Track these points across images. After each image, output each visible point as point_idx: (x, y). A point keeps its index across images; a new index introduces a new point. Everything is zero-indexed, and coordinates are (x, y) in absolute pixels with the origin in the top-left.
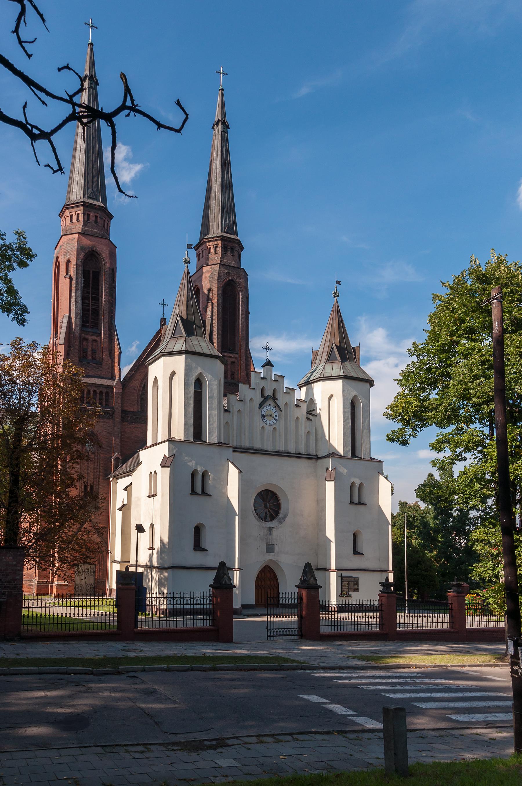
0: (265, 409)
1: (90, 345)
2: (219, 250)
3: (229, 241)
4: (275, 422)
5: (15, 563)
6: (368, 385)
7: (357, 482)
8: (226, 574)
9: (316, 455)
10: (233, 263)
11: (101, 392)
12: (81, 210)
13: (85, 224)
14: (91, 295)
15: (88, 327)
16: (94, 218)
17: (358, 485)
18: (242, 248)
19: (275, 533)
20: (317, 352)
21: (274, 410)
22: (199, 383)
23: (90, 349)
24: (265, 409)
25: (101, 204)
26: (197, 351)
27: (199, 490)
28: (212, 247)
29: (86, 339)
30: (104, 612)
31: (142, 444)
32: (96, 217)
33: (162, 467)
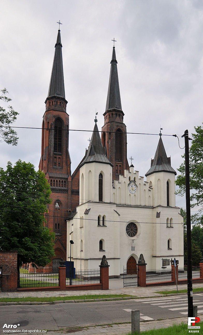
1: (57, 160)
3: (118, 112)
4: (135, 192)
5: (13, 258)
6: (174, 174)
7: (102, 215)
9: (153, 207)
10: (119, 121)
11: (62, 181)
14: (58, 137)
15: (56, 152)
16: (59, 103)
17: (170, 219)
18: (124, 115)
19: (135, 242)
21: (135, 187)
22: (101, 175)
31: (78, 205)
32: (60, 102)
33: (85, 214)
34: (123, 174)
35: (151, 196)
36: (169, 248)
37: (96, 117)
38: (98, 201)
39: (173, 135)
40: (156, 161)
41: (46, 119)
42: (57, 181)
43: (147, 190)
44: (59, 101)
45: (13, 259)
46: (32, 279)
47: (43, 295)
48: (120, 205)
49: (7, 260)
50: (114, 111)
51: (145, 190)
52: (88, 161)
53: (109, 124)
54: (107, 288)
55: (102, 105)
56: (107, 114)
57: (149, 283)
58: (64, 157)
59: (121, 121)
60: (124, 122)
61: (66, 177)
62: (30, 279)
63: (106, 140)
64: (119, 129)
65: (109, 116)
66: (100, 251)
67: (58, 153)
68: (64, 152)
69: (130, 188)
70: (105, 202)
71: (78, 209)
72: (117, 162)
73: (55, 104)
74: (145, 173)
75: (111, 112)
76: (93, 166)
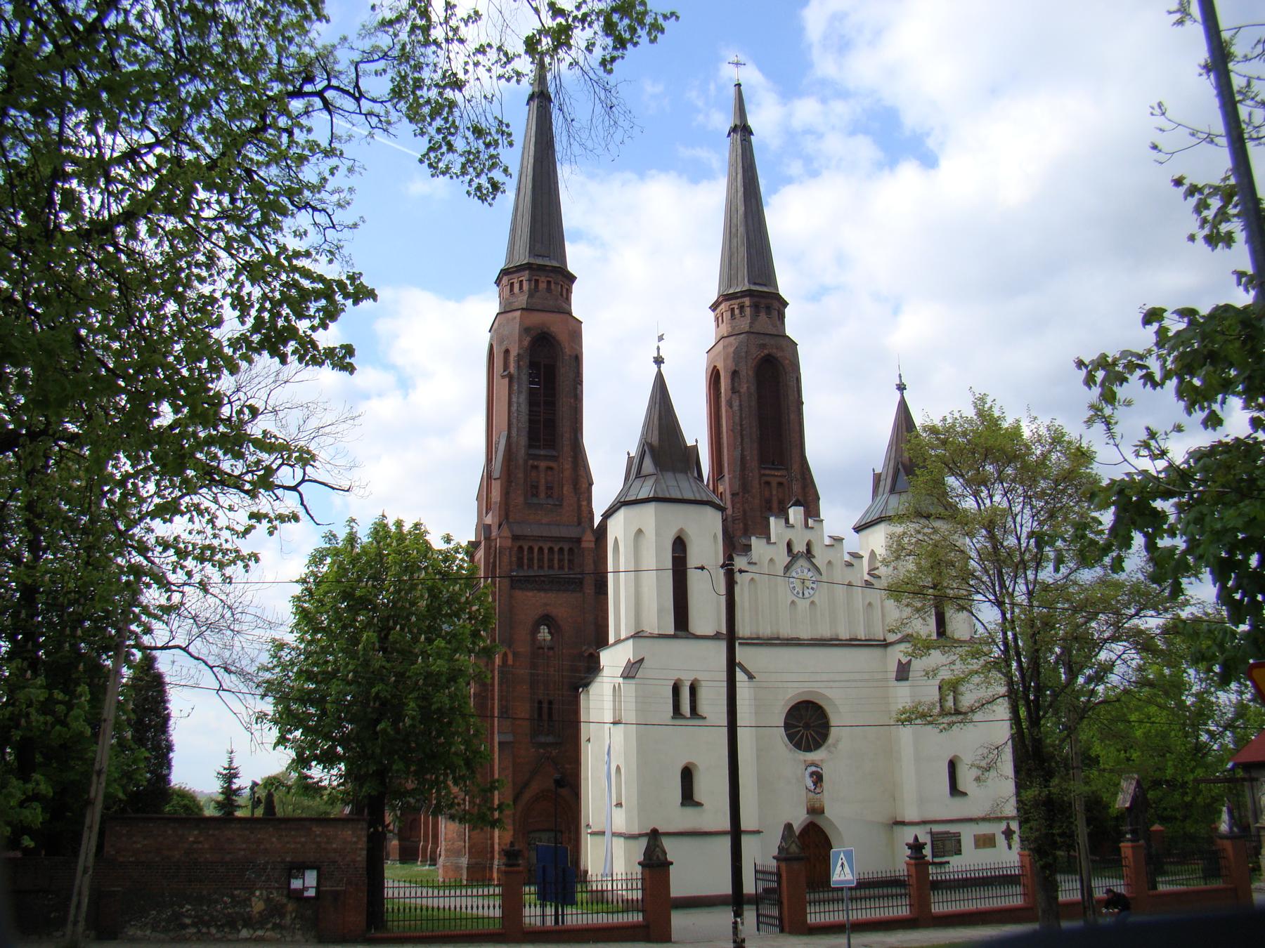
1: (542, 475)
2: (748, 311)
11: (561, 550)
12: (525, 276)
13: (531, 295)
15: (539, 447)
22: (680, 545)
25: (555, 264)
27: (686, 708)
31: (603, 642)
32: (549, 282)
37: (658, 348)
38: (672, 632)
41: (501, 341)
42: (541, 549)
45: (356, 843)
46: (436, 905)
48: (758, 638)
50: (752, 297)
55: (703, 272)
56: (723, 306)
58: (568, 466)
59: (775, 326)
60: (789, 332)
61: (573, 532)
62: (430, 904)
64: (769, 355)
66: (683, 804)
67: (542, 452)
68: (567, 449)
70: (698, 633)
71: (605, 657)
72: (767, 472)
73: (530, 290)
74: (855, 519)
76: (647, 516)
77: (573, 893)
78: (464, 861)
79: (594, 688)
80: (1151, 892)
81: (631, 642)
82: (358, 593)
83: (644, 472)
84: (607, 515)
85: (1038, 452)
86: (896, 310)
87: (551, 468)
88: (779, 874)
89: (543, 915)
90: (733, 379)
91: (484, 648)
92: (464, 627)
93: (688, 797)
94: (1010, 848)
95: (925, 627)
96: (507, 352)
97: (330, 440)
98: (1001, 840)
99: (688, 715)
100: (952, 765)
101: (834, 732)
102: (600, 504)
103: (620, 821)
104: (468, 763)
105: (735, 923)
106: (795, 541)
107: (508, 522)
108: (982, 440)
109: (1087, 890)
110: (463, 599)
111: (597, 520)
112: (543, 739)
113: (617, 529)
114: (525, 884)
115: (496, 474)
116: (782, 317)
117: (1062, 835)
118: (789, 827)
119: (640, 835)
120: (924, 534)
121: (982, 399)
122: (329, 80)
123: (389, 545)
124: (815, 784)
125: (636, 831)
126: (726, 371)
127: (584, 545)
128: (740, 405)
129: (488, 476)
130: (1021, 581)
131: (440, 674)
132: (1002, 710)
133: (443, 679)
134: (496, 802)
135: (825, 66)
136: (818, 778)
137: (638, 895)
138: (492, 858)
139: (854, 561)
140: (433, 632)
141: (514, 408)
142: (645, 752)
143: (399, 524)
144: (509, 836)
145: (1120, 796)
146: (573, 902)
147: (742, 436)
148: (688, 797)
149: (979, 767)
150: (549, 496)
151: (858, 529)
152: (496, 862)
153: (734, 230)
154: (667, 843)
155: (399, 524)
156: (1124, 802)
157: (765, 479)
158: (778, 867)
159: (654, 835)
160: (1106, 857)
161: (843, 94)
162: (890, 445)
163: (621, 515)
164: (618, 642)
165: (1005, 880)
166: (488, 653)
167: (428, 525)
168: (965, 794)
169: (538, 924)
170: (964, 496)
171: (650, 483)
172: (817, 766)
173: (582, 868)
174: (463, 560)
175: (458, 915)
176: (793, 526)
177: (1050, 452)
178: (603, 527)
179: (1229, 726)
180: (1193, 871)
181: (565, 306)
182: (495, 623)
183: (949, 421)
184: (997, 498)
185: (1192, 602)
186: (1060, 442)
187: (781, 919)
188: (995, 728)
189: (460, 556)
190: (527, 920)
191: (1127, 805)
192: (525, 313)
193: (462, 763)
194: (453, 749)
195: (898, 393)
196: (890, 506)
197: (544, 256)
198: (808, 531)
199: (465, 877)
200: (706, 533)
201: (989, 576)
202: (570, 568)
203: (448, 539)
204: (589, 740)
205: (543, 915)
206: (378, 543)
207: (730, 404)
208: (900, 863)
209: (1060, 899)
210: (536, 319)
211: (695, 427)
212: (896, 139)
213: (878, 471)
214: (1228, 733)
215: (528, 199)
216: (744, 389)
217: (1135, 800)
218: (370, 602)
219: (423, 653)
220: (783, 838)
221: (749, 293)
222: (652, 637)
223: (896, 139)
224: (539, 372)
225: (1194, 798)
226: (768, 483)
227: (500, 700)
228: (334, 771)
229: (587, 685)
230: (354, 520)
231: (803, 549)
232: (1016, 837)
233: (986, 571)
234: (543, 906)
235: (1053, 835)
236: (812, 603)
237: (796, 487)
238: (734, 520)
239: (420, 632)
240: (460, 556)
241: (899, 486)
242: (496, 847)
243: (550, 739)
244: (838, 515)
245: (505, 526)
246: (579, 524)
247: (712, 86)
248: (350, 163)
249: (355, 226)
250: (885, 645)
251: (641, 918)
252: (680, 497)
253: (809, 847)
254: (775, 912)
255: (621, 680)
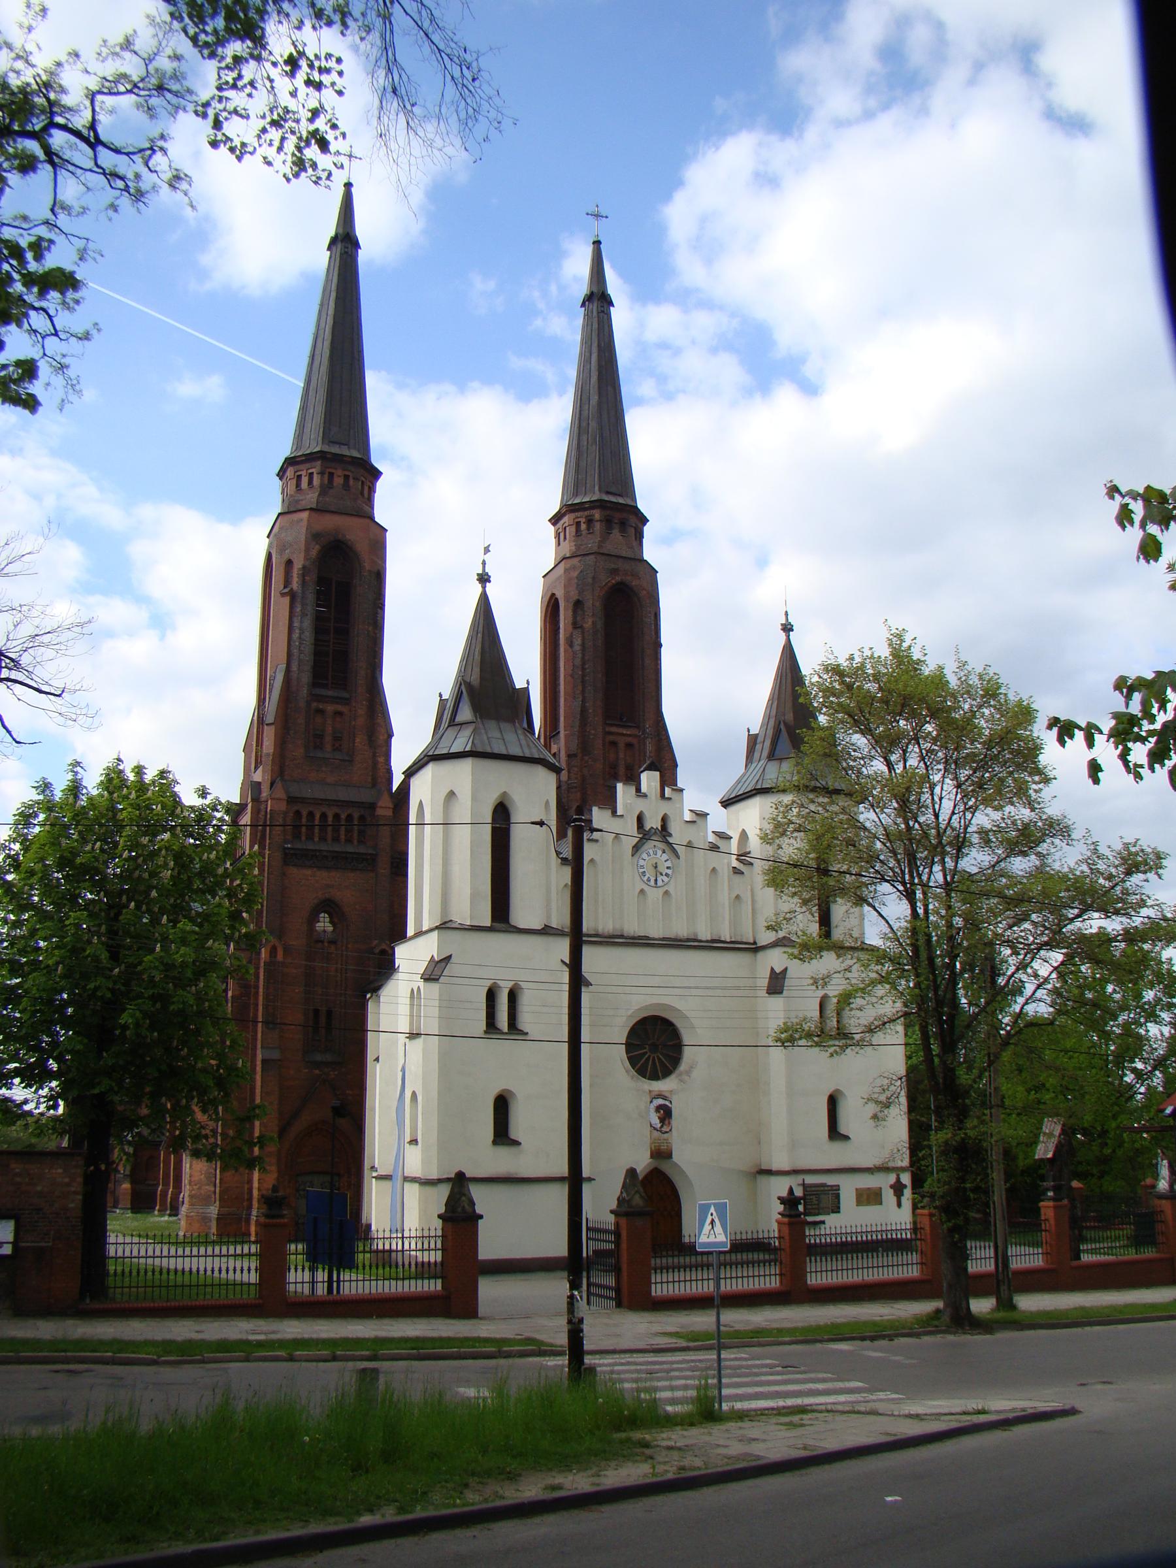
0: (645, 856)
1: (329, 722)
2: (597, 526)
5: (67, 1180)
8: (464, 1195)
9: (755, 943)
10: (629, 554)
11: (349, 818)
13: (324, 490)
20: (756, 736)
22: (502, 814)
23: (329, 729)
24: (645, 856)
25: (355, 454)
26: (496, 751)
28: (583, 520)
29: (320, 712)
30: (388, 1269)
31: (400, 935)
32: (346, 477)
34: (610, 802)
35: (747, 897)
36: (835, 1133)
37: (484, 563)
38: (487, 922)
39: (533, 823)
40: (768, 743)
42: (324, 816)
43: (725, 873)
44: (339, 472)
46: (172, 1267)
47: (182, 1330)
48: (596, 935)
49: (39, 1188)
50: (602, 509)
51: (714, 869)
52: (445, 751)
53: (575, 561)
54: (470, 1311)
57: (734, 1287)
58: (362, 711)
60: (648, 555)
61: (365, 796)
63: (562, 631)
64: (622, 583)
65: (573, 529)
66: (495, 1143)
67: (330, 693)
69: (641, 862)
72: (614, 729)
73: (322, 485)
74: (723, 792)
75: (586, 509)
76: (462, 775)
77: (352, 1253)
78: (213, 1210)
79: (386, 992)
80: (1075, 1263)
81: (436, 933)
82: (78, 860)
83: (459, 719)
84: (410, 773)
85: (966, 707)
86: (762, 562)
87: (340, 714)
88: (617, 1233)
89: (313, 1282)
90: (575, 612)
91: (246, 935)
92: (220, 905)
93: (502, 1134)
94: (899, 1205)
95: (807, 924)
96: (289, 563)
97: (50, 653)
98: (889, 1196)
99: (506, 1030)
100: (833, 1102)
101: (688, 1052)
102: (403, 752)
103: (415, 1162)
104: (220, 1083)
105: (571, 1297)
106: (647, 814)
107: (283, 780)
108: (900, 686)
109: (1002, 1259)
110: (220, 871)
111: (397, 780)
112: (318, 1057)
113: (422, 790)
114: (290, 1241)
115: (270, 718)
116: (639, 536)
117: (976, 1190)
118: (631, 1172)
119: (440, 1181)
120: (820, 804)
121: (900, 636)
122: (51, 118)
123: (126, 797)
124: (662, 1120)
125: (434, 1175)
126: (567, 599)
127: (379, 812)
128: (583, 645)
129: (260, 721)
130: (937, 868)
131: (184, 965)
132: (896, 1035)
133: (189, 974)
134: (257, 1134)
135: (691, 270)
136: (666, 1114)
137: (436, 1257)
138: (250, 1207)
139: (720, 843)
140: (179, 911)
141: (296, 636)
142: (449, 1074)
143: (139, 770)
144: (271, 1178)
145: (1040, 1147)
146: (351, 1265)
147: (583, 682)
148: (502, 1134)
149: (877, 1102)
150: (336, 749)
151: (727, 803)
152: (254, 1212)
153: (584, 424)
154: (476, 1191)
155: (139, 770)
156: (1046, 1151)
157: (612, 738)
158: (617, 1224)
159: (460, 1182)
160: (1024, 1220)
161: (708, 305)
162: (771, 699)
163: (428, 772)
164: (419, 934)
165: (891, 1245)
166: (250, 943)
167: (177, 773)
168: (847, 1138)
169: (307, 1291)
170: (872, 758)
171: (467, 732)
172: (665, 1098)
173: (364, 1221)
174: (221, 820)
175: (209, 1281)
176: (645, 796)
177: (980, 707)
178: (405, 787)
179: (1160, 1063)
180: (1117, 1238)
181: (367, 508)
182: (262, 903)
183: (858, 659)
184: (913, 761)
185: (1149, 902)
186: (995, 696)
187: (618, 1290)
188: (890, 1056)
189: (218, 815)
190: (292, 1288)
191: (1050, 1155)
192: (313, 514)
193: (211, 1083)
194: (200, 1065)
195: (783, 635)
196: (767, 777)
197: (340, 444)
198: (665, 803)
199: (214, 1230)
200: (535, 794)
201: (898, 861)
202: (360, 842)
203: (203, 793)
204: (377, 1059)
205: (313, 1282)
206: (111, 793)
207: (570, 643)
208: (769, 1221)
209: (970, 1270)
210: (329, 522)
211: (525, 664)
212: (765, 360)
213: (755, 730)
214: (1157, 1073)
215: (324, 368)
216: (588, 624)
217: (1058, 1148)
218: (97, 871)
219: (165, 939)
220: (624, 1186)
221: (600, 504)
222: (463, 928)
223: (765, 360)
224: (329, 591)
225: (1114, 1151)
226: (614, 744)
227: (266, 1007)
228: (44, 1092)
229: (376, 990)
230: (78, 764)
231: (657, 824)
232: (908, 1192)
233: (894, 853)
234: (313, 1270)
235: (965, 1188)
236: (666, 893)
237: (650, 747)
238: (569, 789)
239: (163, 911)
240: (218, 815)
241: (778, 753)
242: (255, 1193)
243: (328, 1057)
244: (700, 789)
245: (279, 784)
246: (374, 785)
247: (553, 288)
248: (81, 244)
249: (86, 337)
250: (755, 949)
251: (439, 1287)
252: (504, 752)
253: (655, 1197)
254: (610, 1281)
255: (421, 984)
